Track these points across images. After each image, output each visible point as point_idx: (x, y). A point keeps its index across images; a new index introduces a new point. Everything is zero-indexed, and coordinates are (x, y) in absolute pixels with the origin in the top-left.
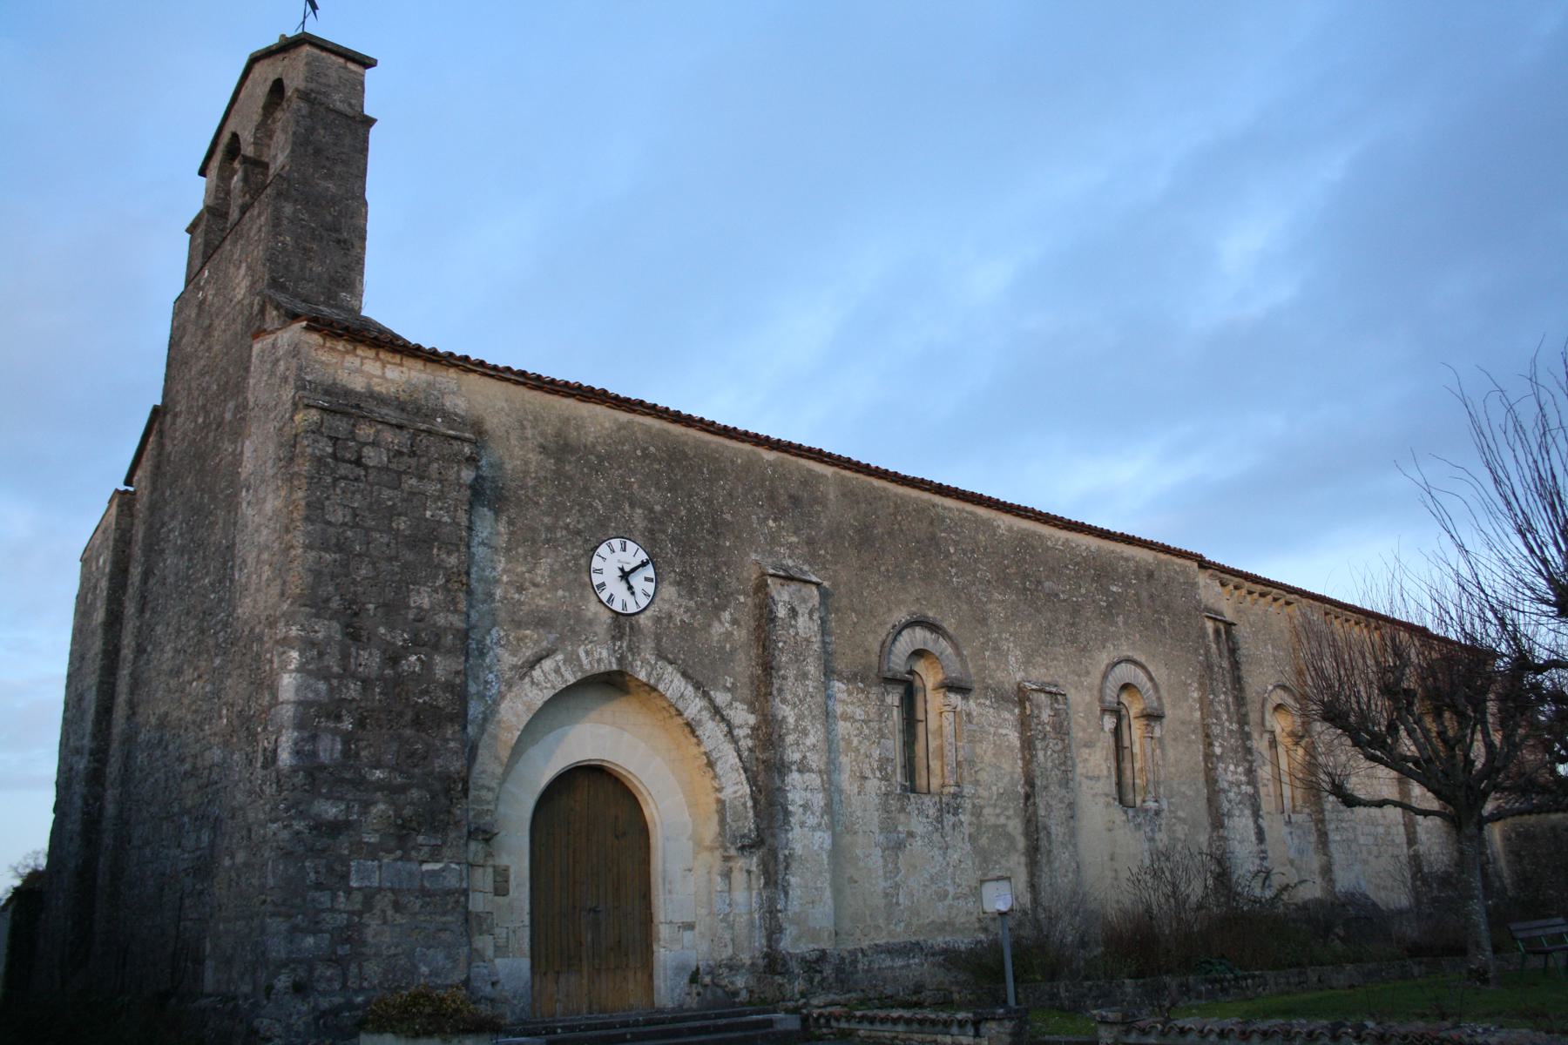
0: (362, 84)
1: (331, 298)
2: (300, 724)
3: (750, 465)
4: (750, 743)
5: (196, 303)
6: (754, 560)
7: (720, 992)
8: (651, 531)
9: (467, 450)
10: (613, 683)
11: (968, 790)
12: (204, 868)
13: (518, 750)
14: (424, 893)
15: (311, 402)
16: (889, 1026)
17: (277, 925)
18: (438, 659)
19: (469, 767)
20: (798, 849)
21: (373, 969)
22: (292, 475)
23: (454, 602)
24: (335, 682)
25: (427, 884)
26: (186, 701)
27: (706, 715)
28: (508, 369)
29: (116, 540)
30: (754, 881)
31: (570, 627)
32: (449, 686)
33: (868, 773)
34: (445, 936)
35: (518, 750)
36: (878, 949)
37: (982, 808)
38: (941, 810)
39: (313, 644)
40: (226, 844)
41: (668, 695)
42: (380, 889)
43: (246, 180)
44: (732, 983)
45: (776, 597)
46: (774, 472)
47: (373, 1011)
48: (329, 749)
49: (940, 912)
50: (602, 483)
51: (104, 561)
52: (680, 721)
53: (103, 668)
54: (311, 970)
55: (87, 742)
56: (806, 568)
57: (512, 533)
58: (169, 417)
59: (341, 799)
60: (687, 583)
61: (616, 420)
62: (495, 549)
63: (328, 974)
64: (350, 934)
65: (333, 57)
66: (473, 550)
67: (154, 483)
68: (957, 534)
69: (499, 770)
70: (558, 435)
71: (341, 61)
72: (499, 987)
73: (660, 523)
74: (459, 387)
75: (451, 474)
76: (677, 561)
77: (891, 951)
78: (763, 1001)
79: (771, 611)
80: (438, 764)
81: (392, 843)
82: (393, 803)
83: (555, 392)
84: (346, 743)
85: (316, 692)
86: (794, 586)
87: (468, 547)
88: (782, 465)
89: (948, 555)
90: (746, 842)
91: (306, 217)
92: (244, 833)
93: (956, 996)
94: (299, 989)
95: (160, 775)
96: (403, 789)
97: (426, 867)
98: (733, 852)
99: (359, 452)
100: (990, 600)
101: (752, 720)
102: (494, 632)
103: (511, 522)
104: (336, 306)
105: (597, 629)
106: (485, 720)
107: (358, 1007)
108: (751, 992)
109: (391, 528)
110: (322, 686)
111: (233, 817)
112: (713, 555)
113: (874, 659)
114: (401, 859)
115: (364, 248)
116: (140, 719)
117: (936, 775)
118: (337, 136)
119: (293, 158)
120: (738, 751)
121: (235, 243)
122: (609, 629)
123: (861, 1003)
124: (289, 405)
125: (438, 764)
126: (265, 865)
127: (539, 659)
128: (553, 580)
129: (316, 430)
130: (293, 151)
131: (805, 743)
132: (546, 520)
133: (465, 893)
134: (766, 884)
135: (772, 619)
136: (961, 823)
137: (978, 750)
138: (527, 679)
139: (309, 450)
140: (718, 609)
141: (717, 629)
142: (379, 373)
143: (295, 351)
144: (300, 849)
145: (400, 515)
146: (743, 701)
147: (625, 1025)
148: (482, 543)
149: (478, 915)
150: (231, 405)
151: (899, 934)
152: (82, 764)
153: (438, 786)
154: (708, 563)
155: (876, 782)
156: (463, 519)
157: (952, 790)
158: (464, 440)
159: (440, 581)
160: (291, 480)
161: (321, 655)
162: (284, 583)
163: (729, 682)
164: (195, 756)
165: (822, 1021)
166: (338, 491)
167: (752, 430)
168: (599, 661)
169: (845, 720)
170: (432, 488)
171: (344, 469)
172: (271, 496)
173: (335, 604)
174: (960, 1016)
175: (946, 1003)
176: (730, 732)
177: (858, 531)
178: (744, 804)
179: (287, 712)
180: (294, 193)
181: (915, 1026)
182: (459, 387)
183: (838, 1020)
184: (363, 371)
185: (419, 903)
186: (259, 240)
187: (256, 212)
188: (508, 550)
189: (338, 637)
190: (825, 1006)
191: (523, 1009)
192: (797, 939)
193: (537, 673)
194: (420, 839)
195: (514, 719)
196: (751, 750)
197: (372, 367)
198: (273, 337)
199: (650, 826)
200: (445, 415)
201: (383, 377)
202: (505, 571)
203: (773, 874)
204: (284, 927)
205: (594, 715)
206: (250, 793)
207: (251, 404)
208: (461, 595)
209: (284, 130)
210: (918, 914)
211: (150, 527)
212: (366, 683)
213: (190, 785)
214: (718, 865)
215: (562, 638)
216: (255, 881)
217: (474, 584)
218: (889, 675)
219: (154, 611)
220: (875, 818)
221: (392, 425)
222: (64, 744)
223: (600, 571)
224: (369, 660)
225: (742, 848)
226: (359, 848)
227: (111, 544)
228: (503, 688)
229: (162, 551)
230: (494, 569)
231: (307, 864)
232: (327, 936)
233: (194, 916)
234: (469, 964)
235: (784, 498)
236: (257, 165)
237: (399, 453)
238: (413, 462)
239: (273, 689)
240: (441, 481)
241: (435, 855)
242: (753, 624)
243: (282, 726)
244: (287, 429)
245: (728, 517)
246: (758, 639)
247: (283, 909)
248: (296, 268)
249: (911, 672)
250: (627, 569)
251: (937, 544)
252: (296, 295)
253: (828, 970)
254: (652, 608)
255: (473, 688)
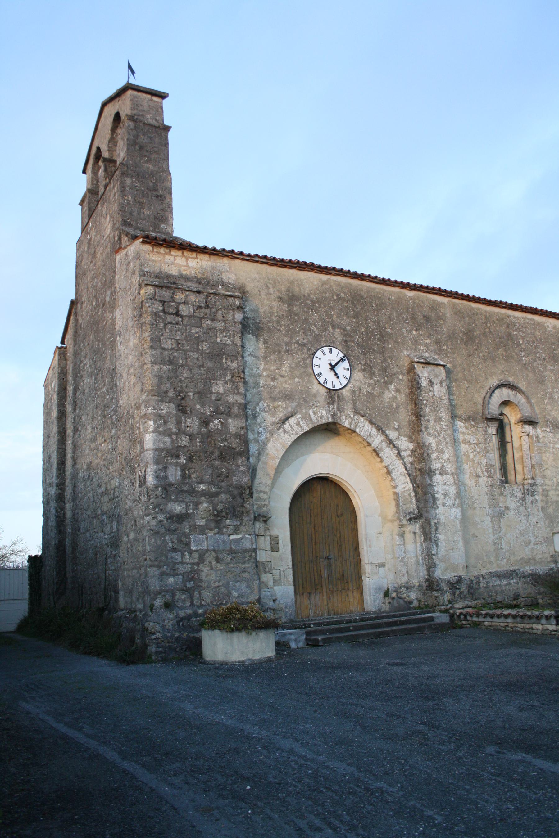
0: (162, 108)
1: (156, 228)
2: (157, 462)
3: (399, 300)
4: (411, 459)
5: (87, 241)
6: (405, 355)
7: (401, 602)
8: (346, 342)
9: (237, 302)
10: (330, 429)
11: (539, 481)
12: (115, 543)
13: (279, 470)
14: (232, 552)
15: (149, 283)
16: (502, 619)
17: (153, 572)
18: (230, 421)
19: (252, 481)
20: (442, 519)
21: (207, 595)
22: (142, 325)
23: (237, 388)
24: (174, 437)
25: (233, 547)
26: (100, 455)
27: (384, 445)
28: (257, 255)
29: (59, 373)
30: (418, 538)
31: (305, 399)
32: (238, 436)
33: (480, 474)
34: (246, 575)
35: (279, 470)
36: (493, 575)
37: (548, 491)
38: (524, 493)
39: (160, 416)
40: (124, 529)
41: (362, 434)
42: (207, 550)
43: (106, 170)
44: (408, 596)
45: (421, 375)
46: (414, 303)
47: (208, 618)
48: (174, 474)
49: (527, 552)
50: (316, 316)
51: (54, 385)
52: (369, 449)
53: (59, 441)
54: (173, 596)
55: (54, 480)
56: (436, 357)
57: (267, 348)
58: (79, 304)
59: (183, 501)
60: (368, 369)
61: (320, 280)
62: (258, 358)
63: (183, 597)
64: (193, 576)
65: (144, 95)
66: (246, 359)
67: (75, 340)
68: (523, 332)
69: (269, 482)
70: (288, 290)
71: (149, 96)
72: (277, 602)
73: (351, 336)
74: (230, 268)
75: (230, 316)
76: (362, 357)
77: (499, 575)
78: (427, 606)
79: (418, 383)
80: (235, 480)
81: (213, 525)
82: (211, 502)
83: (285, 266)
84: (183, 470)
85: (164, 443)
86: (430, 368)
87: (243, 357)
88: (418, 298)
89: (519, 345)
90: (412, 516)
91: (138, 185)
92: (133, 522)
93: (540, 601)
94: (168, 606)
95: (90, 495)
96: (216, 494)
97: (232, 537)
98: (405, 522)
99: (177, 308)
100: (545, 370)
101: (411, 446)
102: (261, 404)
103: (265, 342)
104: (160, 232)
105: (319, 399)
106: (259, 454)
107: (200, 615)
108: (420, 601)
109: (198, 349)
110: (167, 440)
111: (127, 514)
112: (382, 353)
113: (480, 407)
114: (218, 533)
115: (171, 199)
116: (78, 466)
117: (520, 472)
118: (151, 138)
119: (130, 154)
120: (404, 465)
121: (103, 205)
122: (326, 399)
123: (484, 606)
124: (137, 286)
125: (235, 480)
126: (144, 540)
127: (288, 418)
128: (292, 372)
129: (153, 298)
130: (128, 149)
131: (441, 459)
132: (285, 339)
133: (255, 551)
134: (425, 540)
135: (419, 388)
136: (536, 500)
137: (544, 458)
138: (281, 430)
139: (150, 309)
140: (387, 383)
141: (388, 395)
142: (185, 263)
143: (138, 256)
144: (163, 530)
145: (203, 341)
146: (405, 436)
147: (349, 621)
148: (251, 355)
149: (263, 563)
150: (109, 292)
151: (503, 566)
152: (53, 491)
153: (235, 492)
154: (380, 358)
155: (485, 478)
156: (238, 341)
157: (530, 481)
158: (235, 297)
159: (229, 377)
160: (141, 327)
161: (165, 422)
162: (143, 384)
163: (396, 425)
164: (106, 484)
165: (462, 617)
166: (168, 331)
167: (399, 280)
168: (321, 417)
169: (465, 444)
170: (219, 325)
171: (169, 318)
172: (132, 338)
173: (171, 394)
174: (547, 613)
175: (534, 605)
176: (399, 454)
177: (465, 334)
178: (410, 495)
179: (149, 455)
180: (130, 172)
181: (519, 619)
182: (230, 268)
183: (471, 616)
184: (175, 264)
185: (229, 557)
186: (115, 201)
187: (112, 186)
188: (265, 358)
189: (174, 412)
190: (463, 608)
191: (291, 614)
192: (445, 570)
193: (287, 426)
194: (228, 522)
195: (276, 453)
196: (411, 463)
197: (181, 261)
198: (126, 250)
199: (356, 509)
200: (224, 284)
201: (187, 266)
202: (264, 369)
203: (428, 534)
204: (157, 573)
205: (320, 448)
206: (134, 501)
207: (118, 289)
208: (241, 384)
209: (123, 139)
210: (514, 554)
211: (75, 364)
212: (192, 437)
213: (105, 499)
214: (396, 530)
215: (299, 405)
216: (140, 549)
217: (247, 378)
218: (489, 416)
219: (80, 409)
220: (485, 500)
221: (194, 292)
222: (44, 482)
223: (318, 366)
224: (192, 424)
225: (410, 520)
226: (194, 528)
227: (57, 375)
228: (268, 436)
229: (82, 376)
230: (258, 369)
231: (167, 538)
232: (181, 577)
233: (113, 568)
234: (260, 590)
235: (420, 317)
236: (110, 161)
237: (200, 307)
238: (208, 311)
239: (141, 443)
240: (224, 321)
241: (236, 530)
242: (408, 391)
243: (147, 463)
244: (137, 299)
245: (389, 330)
246: (411, 399)
247: (156, 563)
248: (135, 213)
249: (502, 414)
250: (333, 364)
251: (512, 339)
252: (137, 228)
253: (464, 588)
254: (349, 385)
255: (251, 436)
